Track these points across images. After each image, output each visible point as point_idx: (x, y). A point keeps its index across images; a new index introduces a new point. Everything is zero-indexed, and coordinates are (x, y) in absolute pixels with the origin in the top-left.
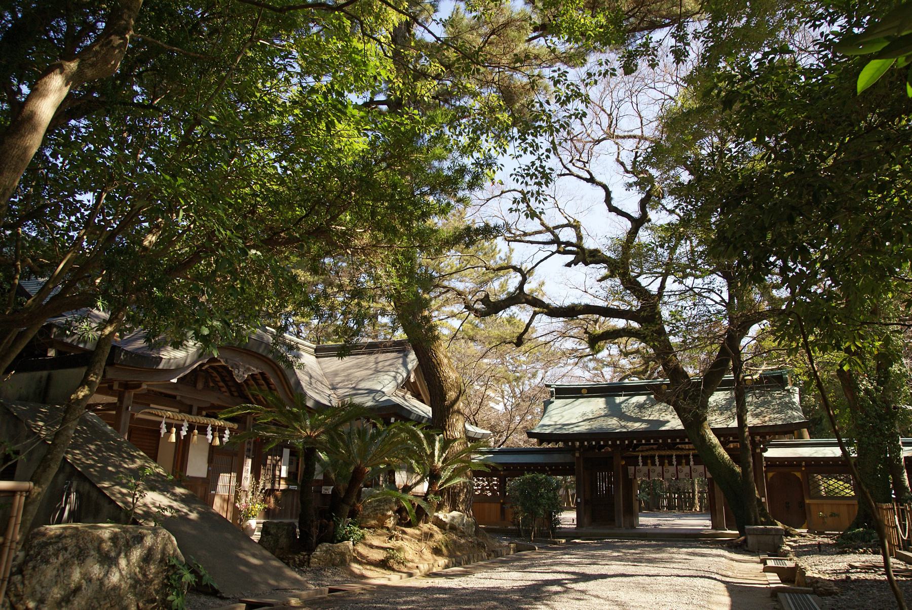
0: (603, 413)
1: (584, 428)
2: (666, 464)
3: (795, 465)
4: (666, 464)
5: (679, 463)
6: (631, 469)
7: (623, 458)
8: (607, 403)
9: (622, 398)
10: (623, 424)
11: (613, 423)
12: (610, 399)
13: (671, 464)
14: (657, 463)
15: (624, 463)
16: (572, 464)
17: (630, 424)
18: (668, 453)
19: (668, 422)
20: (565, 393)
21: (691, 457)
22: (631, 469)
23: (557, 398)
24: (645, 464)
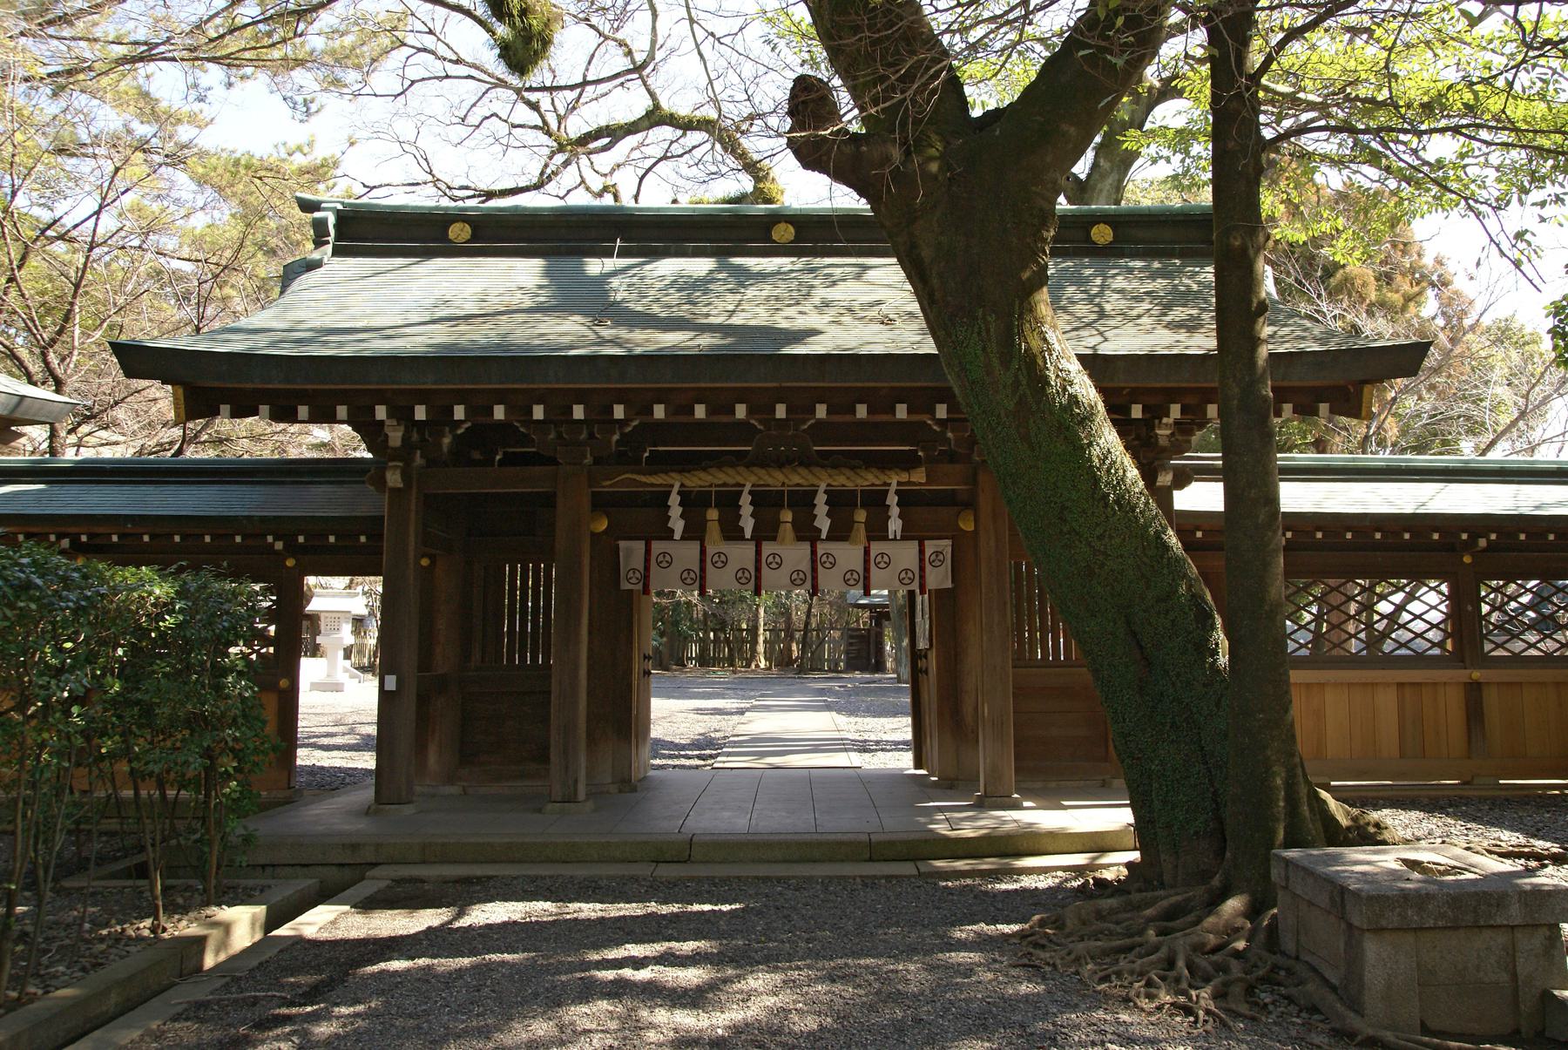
0: (528, 303)
1: (415, 342)
2: (713, 530)
3: (1434, 547)
4: (713, 530)
5: (766, 531)
6: (632, 552)
7: (601, 503)
8: (548, 273)
9: (611, 264)
10: (606, 333)
11: (568, 332)
12: (568, 263)
13: (732, 532)
14: (678, 525)
15: (602, 525)
16: (373, 525)
17: (639, 335)
18: (797, 479)
19: (814, 332)
20: (370, 231)
21: (892, 500)
22: (632, 552)
23: (337, 252)
24: (695, 531)
